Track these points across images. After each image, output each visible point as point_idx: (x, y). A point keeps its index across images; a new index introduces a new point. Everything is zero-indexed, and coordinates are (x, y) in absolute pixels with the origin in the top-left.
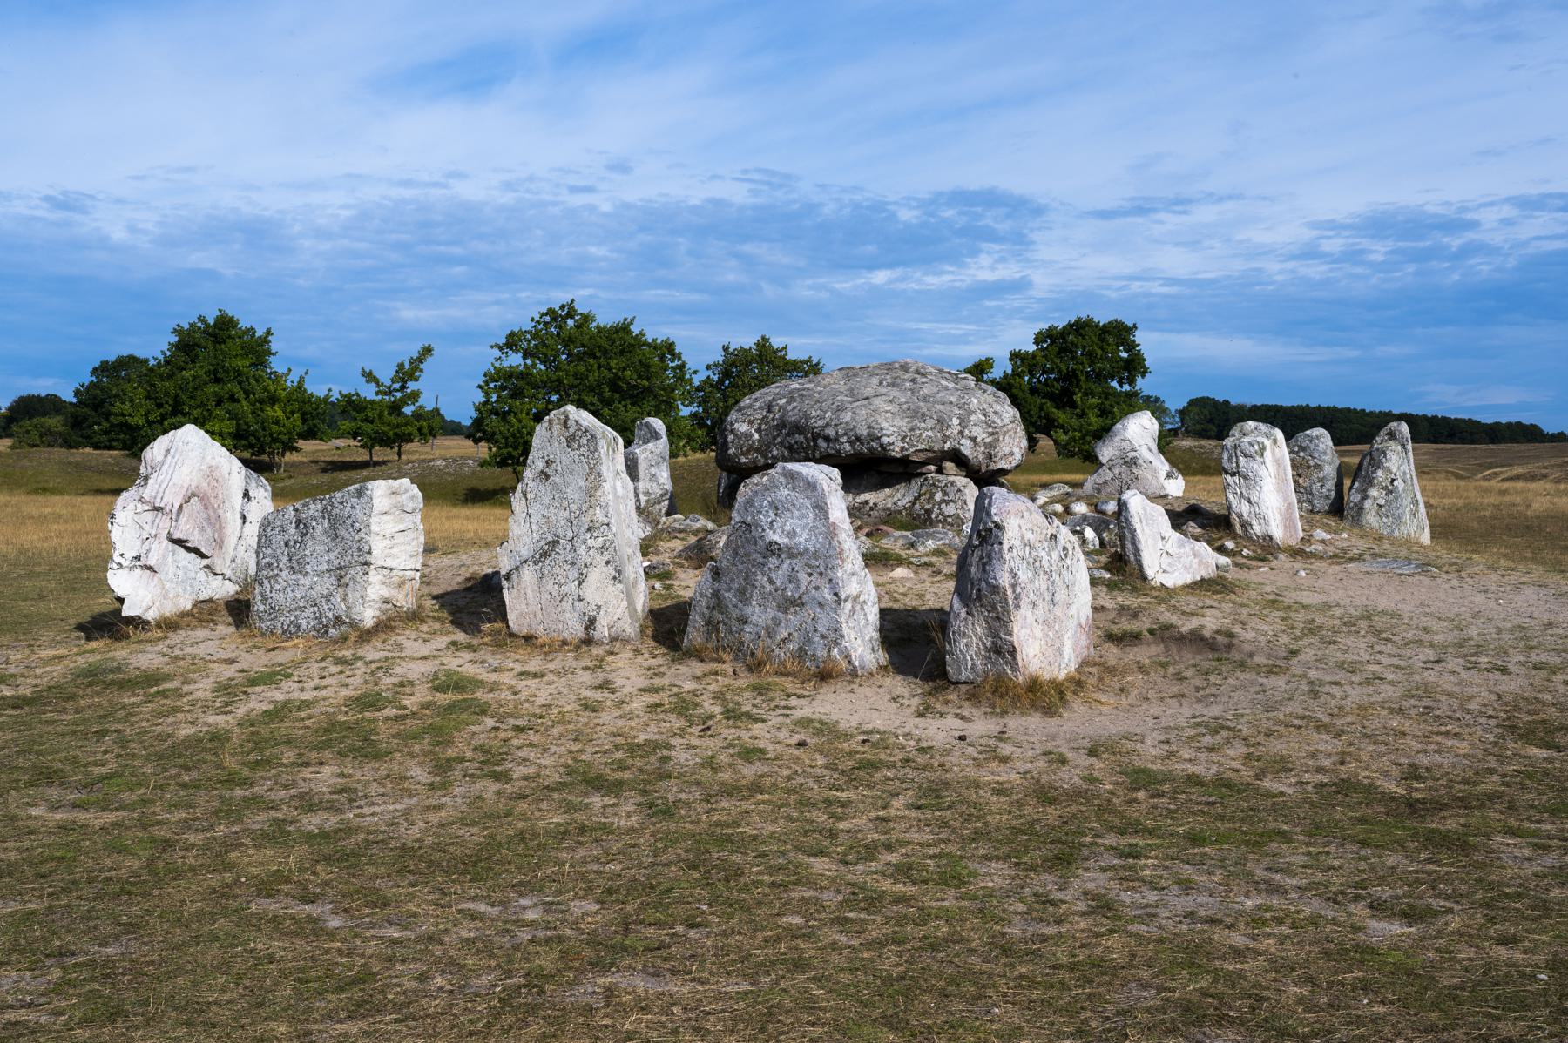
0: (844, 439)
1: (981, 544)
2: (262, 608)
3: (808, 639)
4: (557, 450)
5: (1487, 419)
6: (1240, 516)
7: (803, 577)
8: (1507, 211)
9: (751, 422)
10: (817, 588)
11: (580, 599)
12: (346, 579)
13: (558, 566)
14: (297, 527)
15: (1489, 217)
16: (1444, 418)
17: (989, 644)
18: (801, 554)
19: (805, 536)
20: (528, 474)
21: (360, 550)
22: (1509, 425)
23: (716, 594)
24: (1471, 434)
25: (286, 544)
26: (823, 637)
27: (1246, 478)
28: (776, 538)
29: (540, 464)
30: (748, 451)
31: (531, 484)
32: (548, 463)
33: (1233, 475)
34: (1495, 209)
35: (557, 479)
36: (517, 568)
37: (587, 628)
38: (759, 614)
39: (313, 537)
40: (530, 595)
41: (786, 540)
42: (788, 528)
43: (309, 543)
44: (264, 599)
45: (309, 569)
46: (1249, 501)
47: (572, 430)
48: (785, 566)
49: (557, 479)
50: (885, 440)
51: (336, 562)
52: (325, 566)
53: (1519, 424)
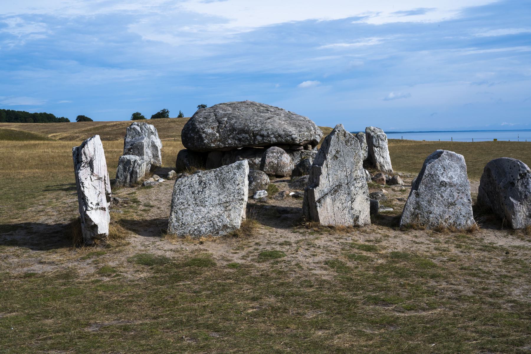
0: (272, 136)
1: (521, 178)
2: (176, 224)
3: (458, 218)
4: (341, 147)
5: (32, 111)
6: (380, 163)
7: (456, 194)
8: (19, 20)
9: (213, 128)
10: (461, 198)
11: (352, 209)
12: (230, 207)
13: (342, 196)
14: (200, 184)
15: (12, 23)
16: (13, 111)
17: (527, 214)
18: (455, 186)
19: (456, 178)
20: (329, 157)
21: (238, 193)
22: (41, 114)
23: (417, 203)
24: (25, 118)
25: (193, 193)
26: (464, 216)
27: (382, 148)
28: (444, 180)
29: (334, 152)
30: (215, 141)
31: (330, 161)
32: (337, 152)
33: (377, 147)
34: (14, 19)
35: (341, 159)
36: (323, 197)
37: (355, 221)
38: (437, 210)
39: (210, 189)
40: (329, 209)
41: (449, 180)
42: (449, 175)
43: (207, 192)
44: (178, 220)
45: (207, 203)
46: (383, 157)
47: (347, 138)
48: (448, 190)
49: (341, 159)
50: (294, 136)
51: (224, 200)
52: (217, 202)
53: (45, 114)
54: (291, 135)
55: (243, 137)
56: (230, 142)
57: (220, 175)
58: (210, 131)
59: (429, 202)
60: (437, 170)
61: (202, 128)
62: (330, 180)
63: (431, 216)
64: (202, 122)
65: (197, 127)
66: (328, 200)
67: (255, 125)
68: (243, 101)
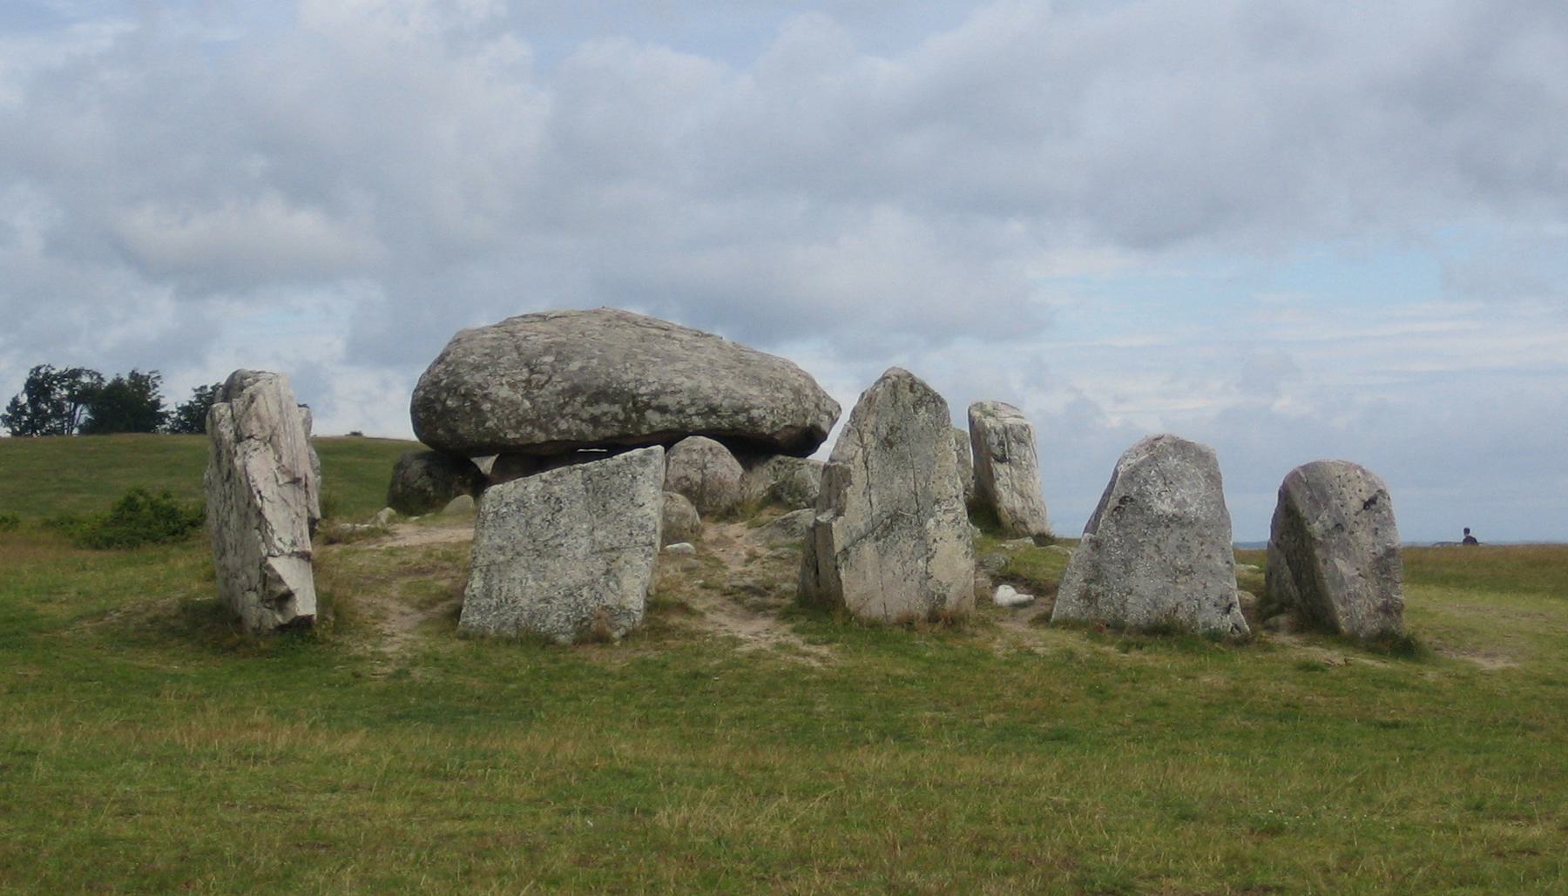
7: (1195, 544)
9: (512, 386)
11: (929, 577)
30: (519, 423)
42: (1178, 497)
46: (1022, 495)
50: (755, 413)
54: (747, 410)
55: (605, 414)
56: (563, 425)
57: (596, 479)
58: (505, 392)
59: (1126, 563)
60: (1146, 482)
61: (479, 386)
62: (874, 500)
63: (1131, 599)
64: (477, 368)
65: (465, 383)
66: (868, 549)
67: (651, 377)
68: (592, 308)
